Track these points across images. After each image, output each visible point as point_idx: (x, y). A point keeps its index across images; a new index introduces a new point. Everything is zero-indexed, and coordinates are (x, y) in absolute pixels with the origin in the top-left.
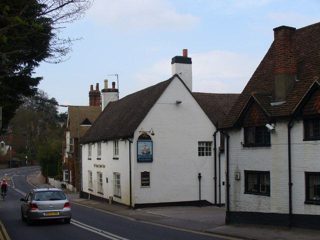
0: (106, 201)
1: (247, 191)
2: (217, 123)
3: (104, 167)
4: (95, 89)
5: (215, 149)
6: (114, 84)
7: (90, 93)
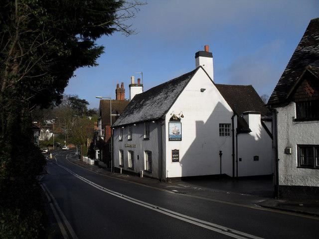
4: (120, 87)
5: (233, 130)
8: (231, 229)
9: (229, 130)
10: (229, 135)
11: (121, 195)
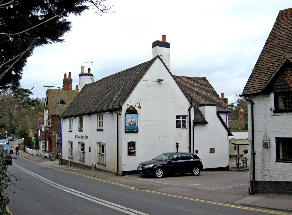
0: (89, 168)
1: (278, 160)
2: (191, 99)
3: (87, 137)
4: (68, 77)
5: (190, 122)
6: (89, 70)
7: (64, 80)
8: (129, 209)
9: (185, 121)
10: (185, 126)
11: (79, 192)
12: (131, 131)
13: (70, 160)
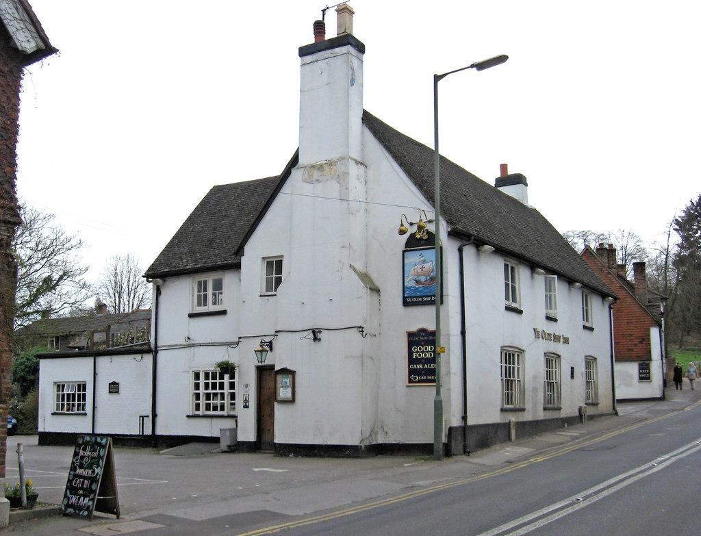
3: (566, 341)
12: (420, 299)
13: (513, 418)
